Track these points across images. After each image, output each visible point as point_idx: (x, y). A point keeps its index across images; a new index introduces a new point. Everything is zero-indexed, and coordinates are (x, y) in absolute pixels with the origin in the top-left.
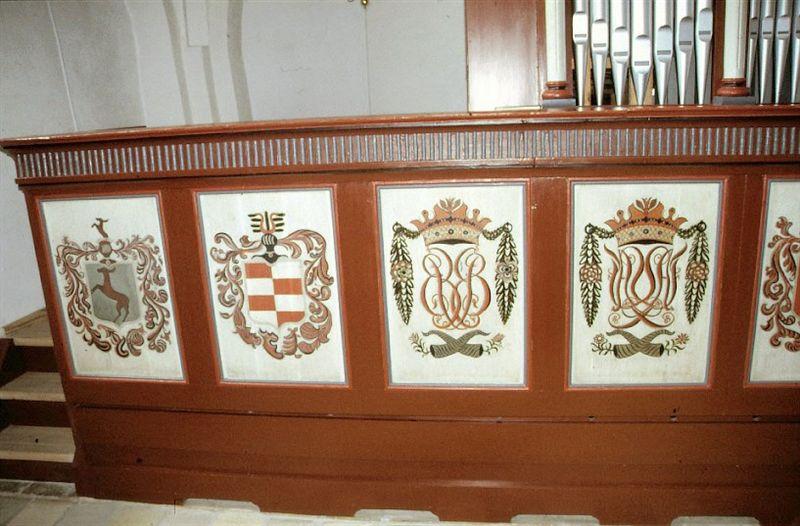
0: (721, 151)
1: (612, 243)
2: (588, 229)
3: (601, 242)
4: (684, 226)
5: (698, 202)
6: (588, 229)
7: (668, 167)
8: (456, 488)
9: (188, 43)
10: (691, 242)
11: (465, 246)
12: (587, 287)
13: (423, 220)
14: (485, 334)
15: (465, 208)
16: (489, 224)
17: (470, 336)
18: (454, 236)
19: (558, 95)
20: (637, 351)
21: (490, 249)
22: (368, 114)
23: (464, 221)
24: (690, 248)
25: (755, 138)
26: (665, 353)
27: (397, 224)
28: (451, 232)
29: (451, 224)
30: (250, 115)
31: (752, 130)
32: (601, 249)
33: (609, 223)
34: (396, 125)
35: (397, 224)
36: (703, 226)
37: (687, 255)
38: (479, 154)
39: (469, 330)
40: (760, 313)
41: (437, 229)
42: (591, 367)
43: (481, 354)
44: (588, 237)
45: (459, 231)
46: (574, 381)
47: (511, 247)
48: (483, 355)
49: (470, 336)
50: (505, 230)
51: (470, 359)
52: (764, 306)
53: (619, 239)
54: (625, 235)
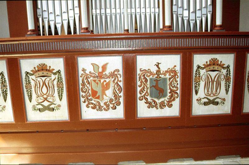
1: (33, 77)
4: (54, 71)
10: (57, 76)
18: (214, 69)
20: (210, 104)
21: (224, 72)
23: (47, 70)
24: (57, 78)
26: (219, 104)
36: (60, 71)
37: (56, 80)
39: (215, 97)
41: (39, 73)
54: (37, 74)
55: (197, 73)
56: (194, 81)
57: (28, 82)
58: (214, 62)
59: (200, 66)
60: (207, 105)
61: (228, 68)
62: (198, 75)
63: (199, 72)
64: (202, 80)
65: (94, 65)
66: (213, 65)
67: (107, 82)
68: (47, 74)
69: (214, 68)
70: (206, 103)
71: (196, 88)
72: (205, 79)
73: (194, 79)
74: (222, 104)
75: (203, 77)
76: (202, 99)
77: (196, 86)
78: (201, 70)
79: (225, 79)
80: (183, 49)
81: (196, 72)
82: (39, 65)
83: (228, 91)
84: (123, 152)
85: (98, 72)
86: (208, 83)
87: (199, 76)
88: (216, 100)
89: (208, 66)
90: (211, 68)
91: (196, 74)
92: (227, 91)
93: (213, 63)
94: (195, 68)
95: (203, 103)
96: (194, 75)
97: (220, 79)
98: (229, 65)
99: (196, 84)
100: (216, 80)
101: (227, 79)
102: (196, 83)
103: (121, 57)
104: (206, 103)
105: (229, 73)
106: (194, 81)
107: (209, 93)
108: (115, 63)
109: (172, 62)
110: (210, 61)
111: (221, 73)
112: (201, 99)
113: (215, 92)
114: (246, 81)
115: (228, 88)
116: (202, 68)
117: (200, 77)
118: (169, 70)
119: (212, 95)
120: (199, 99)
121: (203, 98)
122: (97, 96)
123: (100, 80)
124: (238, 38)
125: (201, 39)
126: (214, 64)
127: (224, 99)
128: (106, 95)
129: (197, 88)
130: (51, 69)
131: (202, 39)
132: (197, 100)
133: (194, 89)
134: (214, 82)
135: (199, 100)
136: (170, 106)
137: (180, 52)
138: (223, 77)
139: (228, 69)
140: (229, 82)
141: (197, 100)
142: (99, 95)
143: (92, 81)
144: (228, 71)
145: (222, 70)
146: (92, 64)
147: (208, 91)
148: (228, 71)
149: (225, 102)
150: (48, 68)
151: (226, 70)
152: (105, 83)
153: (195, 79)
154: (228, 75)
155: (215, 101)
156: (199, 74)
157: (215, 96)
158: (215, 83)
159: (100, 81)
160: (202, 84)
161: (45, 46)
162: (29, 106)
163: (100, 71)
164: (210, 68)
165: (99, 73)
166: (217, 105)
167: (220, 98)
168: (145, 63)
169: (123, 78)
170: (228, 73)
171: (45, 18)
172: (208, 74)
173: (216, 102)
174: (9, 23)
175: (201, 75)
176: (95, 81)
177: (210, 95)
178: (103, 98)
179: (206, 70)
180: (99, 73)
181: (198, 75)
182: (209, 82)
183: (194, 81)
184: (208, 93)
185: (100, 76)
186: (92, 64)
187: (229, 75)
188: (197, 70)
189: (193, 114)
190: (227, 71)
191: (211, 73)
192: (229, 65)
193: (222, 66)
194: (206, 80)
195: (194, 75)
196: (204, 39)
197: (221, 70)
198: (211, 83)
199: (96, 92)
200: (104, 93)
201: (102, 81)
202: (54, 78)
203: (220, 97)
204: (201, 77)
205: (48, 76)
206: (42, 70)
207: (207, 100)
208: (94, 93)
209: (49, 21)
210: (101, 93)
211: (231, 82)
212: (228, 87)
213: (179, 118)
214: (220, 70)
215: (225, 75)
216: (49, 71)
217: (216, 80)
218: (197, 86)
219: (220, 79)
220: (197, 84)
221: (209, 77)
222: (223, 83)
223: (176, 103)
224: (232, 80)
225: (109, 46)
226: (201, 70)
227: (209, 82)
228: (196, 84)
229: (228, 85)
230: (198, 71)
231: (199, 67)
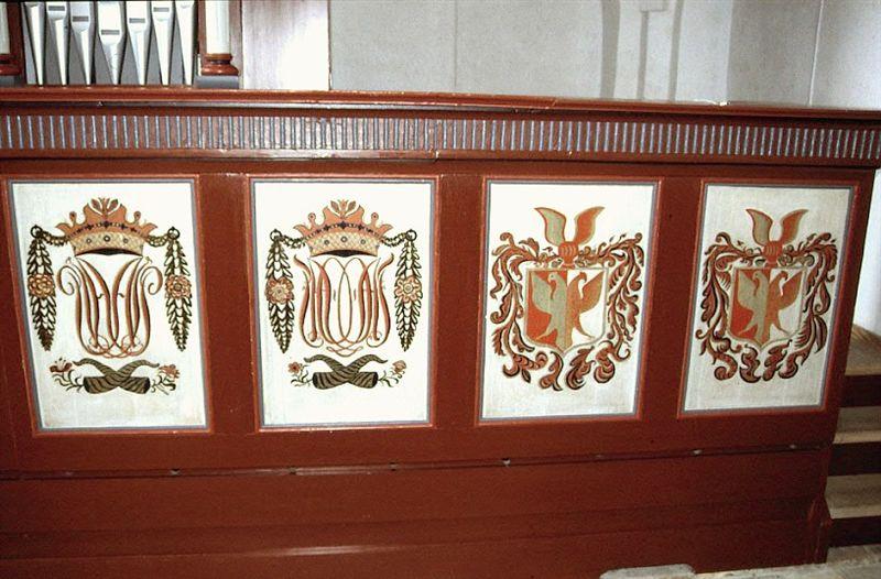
0: (592, 147)
1: (303, 253)
2: (34, 231)
3: (288, 251)
4: (390, 234)
5: (408, 206)
6: (34, 231)
7: (637, 166)
8: (286, 558)
9: (659, 11)
10: (398, 251)
11: (130, 257)
12: (174, 303)
13: (309, 226)
14: (382, 362)
15: (361, 210)
16: (155, 230)
17: (135, 366)
18: (111, 245)
19: (220, 71)
20: (115, 386)
21: (157, 256)
22: (253, 88)
23: (360, 227)
24: (397, 259)
25: (584, 132)
26: (151, 389)
27: (276, 231)
28: (107, 239)
29: (344, 232)
30: (612, 94)
31: (635, 125)
32: (291, 261)
33: (60, 226)
34: (152, 101)
35: (276, 231)
36: (175, 232)
37: (393, 268)
38: (350, 143)
39: (130, 360)
40: (694, 339)
41: (327, 236)
42: (288, 403)
43: (374, 383)
44: (274, 247)
45: (354, 240)
46: (268, 421)
47: (413, 258)
48: (149, 392)
49: (135, 366)
50: (172, 237)
51: (135, 397)
52: (699, 332)
53: (311, 249)
54: (318, 242)
55: (35, 261)
56: (27, 291)
57: (409, 273)
58: (106, 216)
59: (45, 229)
60: (100, 391)
61: (171, 243)
62: (41, 270)
63: (42, 255)
64: (61, 287)
65: (542, 211)
66: (344, 232)
67: (590, 278)
68: (327, 242)
69: (344, 240)
70: (96, 382)
71: (41, 320)
72: (74, 285)
73: (26, 283)
74: (168, 389)
75: (66, 278)
76: (74, 367)
77: (39, 313)
78: (50, 249)
79: (164, 287)
80: (810, 166)
81: (31, 254)
82: (91, 206)
83: (185, 338)
84: (370, 549)
85: (764, 242)
86: (92, 304)
87: (46, 272)
88: (138, 373)
89: (79, 231)
90: (98, 239)
91: (31, 264)
92: (181, 338)
93: (103, 221)
94: (25, 240)
95: (81, 382)
96: (25, 267)
97: (143, 286)
98: (173, 229)
99: (40, 306)
100: (123, 289)
101: (174, 285)
102: (38, 301)
103: (492, 185)
104: (96, 382)
105: (181, 262)
106: (27, 291)
107: (102, 342)
108: (627, 210)
109: (627, 210)
110: (86, 209)
111: (144, 261)
112: (68, 366)
113: (127, 341)
114: (833, 297)
115: (184, 326)
116: (57, 238)
117: (51, 275)
118: (603, 248)
119: (115, 351)
120: (61, 365)
121: (78, 360)
122: (548, 332)
123: (769, 272)
124: (844, 130)
125: (777, 127)
126: (106, 224)
127: (173, 367)
128: (581, 330)
129: (45, 319)
130: (142, 222)
131: (626, 124)
132: (54, 369)
133: (31, 325)
134: (115, 299)
135: (60, 368)
136: (606, 374)
137: (850, 179)
138: (152, 278)
139: (175, 247)
140: (184, 301)
141: (54, 369)
142: (556, 330)
143: (741, 275)
144: (175, 254)
145: (148, 250)
146: (537, 209)
147: (95, 335)
148: (175, 254)
149: (176, 382)
150: (367, 220)
151: (164, 250)
152: (581, 284)
153: (30, 284)
154: (177, 272)
155: (132, 375)
156: (44, 263)
157: (130, 354)
158: (121, 303)
159: (564, 275)
160: (65, 305)
161: (691, 138)
162: (274, 364)
163: (567, 240)
164: (89, 241)
165: (564, 245)
166: (145, 392)
167: (153, 366)
168: (728, 211)
169: (841, 271)
170: (177, 262)
171: (77, 19)
172: (83, 264)
173: (137, 379)
174: (616, 48)
175: (55, 268)
176: (749, 273)
177: (105, 352)
178: (766, 338)
179: (75, 248)
180: (564, 245)
181: (41, 270)
182: (97, 299)
183: (30, 294)
184: (97, 345)
185: (573, 254)
186: (537, 209)
187: (182, 271)
188: (33, 248)
189: (44, 426)
190: (169, 254)
191: (98, 261)
192: (173, 229)
193: (380, 234)
194: (79, 288)
195: (25, 267)
196: (661, 126)
197: (142, 247)
198: (102, 303)
199: (547, 318)
200: (772, 317)
201: (572, 274)
202: (389, 257)
203: (152, 362)
204: (55, 277)
205: (129, 249)
206: (343, 226)
207: (96, 373)
208: (538, 321)
209: (69, 28)
210: (763, 320)
211: (194, 301)
212: (181, 320)
213: (637, 422)
214: (137, 250)
215: (163, 270)
216: (133, 230)
217: (123, 289)
218: (44, 312)
219: (143, 286)
220: (44, 303)
221: (90, 280)
222: (158, 304)
223: (628, 373)
224: (194, 290)
225: (308, 142)
226: (50, 249)
227: (97, 299)
228: (40, 306)
229: (180, 312)
230: (38, 253)
231: (278, 239)
